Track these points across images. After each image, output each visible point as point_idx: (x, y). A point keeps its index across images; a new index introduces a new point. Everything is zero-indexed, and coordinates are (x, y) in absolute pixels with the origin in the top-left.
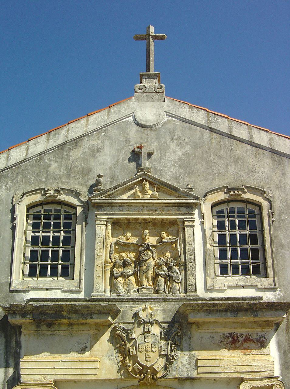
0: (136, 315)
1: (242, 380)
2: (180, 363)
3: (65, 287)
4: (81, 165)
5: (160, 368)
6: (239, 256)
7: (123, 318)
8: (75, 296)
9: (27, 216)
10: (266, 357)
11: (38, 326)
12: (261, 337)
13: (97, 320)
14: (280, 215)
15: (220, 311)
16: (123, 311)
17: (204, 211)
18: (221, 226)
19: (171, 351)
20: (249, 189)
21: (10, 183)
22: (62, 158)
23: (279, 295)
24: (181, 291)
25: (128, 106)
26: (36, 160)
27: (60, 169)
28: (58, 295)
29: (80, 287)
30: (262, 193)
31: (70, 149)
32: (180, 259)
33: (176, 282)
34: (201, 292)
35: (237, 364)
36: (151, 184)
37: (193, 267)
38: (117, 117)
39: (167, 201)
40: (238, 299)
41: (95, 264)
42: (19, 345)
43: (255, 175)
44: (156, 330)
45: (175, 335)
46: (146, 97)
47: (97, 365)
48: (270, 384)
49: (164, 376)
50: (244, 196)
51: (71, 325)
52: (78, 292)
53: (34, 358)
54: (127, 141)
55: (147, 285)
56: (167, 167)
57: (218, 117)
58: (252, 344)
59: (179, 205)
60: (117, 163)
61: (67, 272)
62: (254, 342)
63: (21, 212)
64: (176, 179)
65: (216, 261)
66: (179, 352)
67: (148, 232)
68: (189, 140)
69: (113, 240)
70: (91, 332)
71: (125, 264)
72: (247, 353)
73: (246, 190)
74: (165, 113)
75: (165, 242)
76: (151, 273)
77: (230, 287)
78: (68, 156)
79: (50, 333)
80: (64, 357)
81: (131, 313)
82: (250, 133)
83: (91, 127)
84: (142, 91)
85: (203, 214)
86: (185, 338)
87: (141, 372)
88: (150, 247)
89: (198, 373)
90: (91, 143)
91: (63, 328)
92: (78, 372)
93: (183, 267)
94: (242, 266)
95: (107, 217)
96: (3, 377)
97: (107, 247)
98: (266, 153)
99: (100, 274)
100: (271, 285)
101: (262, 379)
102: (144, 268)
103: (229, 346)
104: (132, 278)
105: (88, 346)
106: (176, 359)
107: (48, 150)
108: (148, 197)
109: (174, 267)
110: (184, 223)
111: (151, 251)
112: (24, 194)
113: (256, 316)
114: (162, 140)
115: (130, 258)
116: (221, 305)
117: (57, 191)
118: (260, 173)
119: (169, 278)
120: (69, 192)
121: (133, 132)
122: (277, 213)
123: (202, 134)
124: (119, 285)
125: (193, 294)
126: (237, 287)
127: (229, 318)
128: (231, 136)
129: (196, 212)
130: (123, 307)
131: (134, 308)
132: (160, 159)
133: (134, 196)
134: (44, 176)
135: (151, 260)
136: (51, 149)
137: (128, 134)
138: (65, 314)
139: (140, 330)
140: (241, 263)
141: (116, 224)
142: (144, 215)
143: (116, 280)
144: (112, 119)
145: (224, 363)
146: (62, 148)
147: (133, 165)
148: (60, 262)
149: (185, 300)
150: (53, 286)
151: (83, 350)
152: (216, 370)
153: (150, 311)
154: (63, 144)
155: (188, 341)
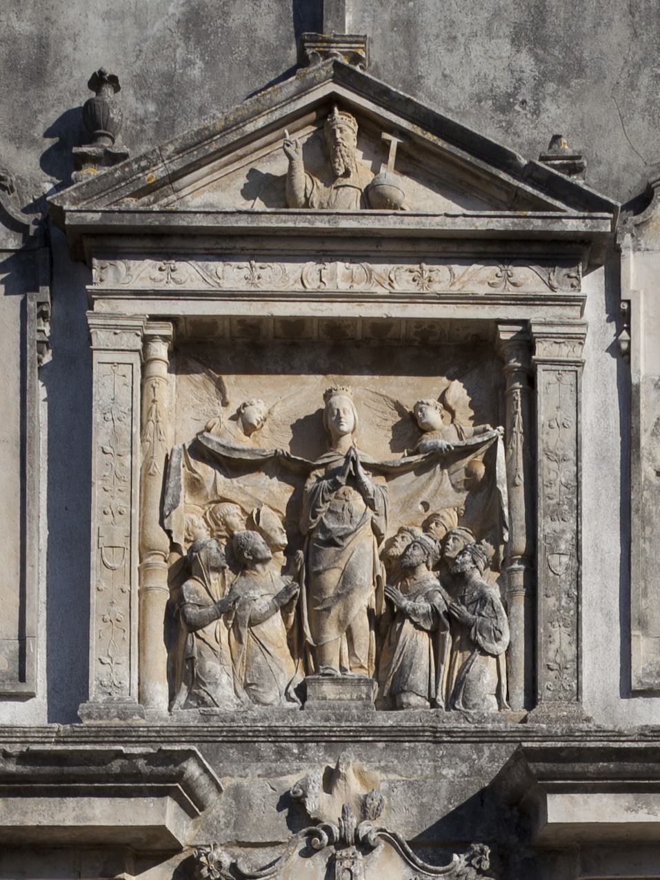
0: (293, 805)
17: (632, 286)
24: (508, 699)
29: (22, 678)
32: (506, 538)
36: (370, 130)
55: (346, 664)
76: (364, 599)
85: (629, 302)
88: (360, 469)
97: (147, 472)
99: (120, 503)
108: (350, 199)
110: (531, 349)
115: (262, 532)
124: (211, 665)
131: (283, 774)
143: (198, 636)
149: (527, 734)
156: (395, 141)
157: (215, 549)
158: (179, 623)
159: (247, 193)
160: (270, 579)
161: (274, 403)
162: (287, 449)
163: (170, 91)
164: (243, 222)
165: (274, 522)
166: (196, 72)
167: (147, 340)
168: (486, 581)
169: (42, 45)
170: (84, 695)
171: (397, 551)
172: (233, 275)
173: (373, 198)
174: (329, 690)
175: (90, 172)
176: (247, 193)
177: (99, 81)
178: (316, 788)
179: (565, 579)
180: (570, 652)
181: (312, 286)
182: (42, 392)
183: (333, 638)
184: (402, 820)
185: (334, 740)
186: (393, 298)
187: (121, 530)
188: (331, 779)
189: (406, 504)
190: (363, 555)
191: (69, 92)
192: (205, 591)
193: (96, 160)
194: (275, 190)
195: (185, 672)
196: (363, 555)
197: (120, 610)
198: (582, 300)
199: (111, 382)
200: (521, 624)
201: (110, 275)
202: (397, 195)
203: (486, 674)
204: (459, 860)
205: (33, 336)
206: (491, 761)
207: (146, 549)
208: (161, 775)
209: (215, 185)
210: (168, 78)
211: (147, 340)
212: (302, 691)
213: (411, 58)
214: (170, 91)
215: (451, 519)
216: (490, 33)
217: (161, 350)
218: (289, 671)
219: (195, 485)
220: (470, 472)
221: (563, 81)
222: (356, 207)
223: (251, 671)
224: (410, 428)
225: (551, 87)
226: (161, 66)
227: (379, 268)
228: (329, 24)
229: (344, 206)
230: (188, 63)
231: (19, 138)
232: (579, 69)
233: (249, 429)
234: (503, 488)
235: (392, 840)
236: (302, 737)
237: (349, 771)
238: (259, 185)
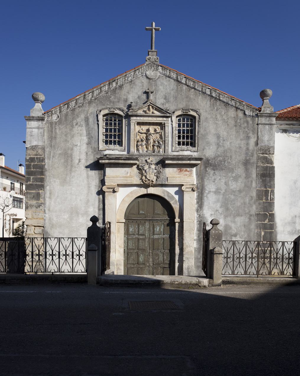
0: (146, 161)
47: (132, 179)
76: (152, 144)
97: (135, 134)
99: (133, 136)
108: (151, 113)
124: (140, 149)
152: (174, 181)
156: (154, 108)
157: (140, 140)
158: (137, 146)
159: (143, 112)
160: (144, 142)
161: (144, 128)
162: (146, 132)
163: (137, 103)
164: (143, 115)
165: (145, 138)
166: (139, 101)
167: (135, 123)
168: (161, 143)
169: (127, 99)
170: (130, 152)
171: (154, 140)
172: (142, 118)
173: (153, 113)
174: (149, 151)
175: (131, 110)
176: (143, 112)
177: (131, 103)
178: (148, 159)
179: (167, 143)
180: (168, 149)
181: (148, 119)
182: (127, 127)
183: (149, 147)
184: (154, 162)
185: (149, 156)
186: (154, 120)
187: (133, 139)
188: (149, 159)
189: (155, 136)
190: (152, 141)
191: (129, 103)
192: (139, 143)
193: (131, 109)
194: (145, 112)
195: (138, 150)
196: (152, 141)
197: (133, 145)
198: (169, 121)
199: (132, 127)
200: (164, 146)
201: (132, 118)
202: (155, 113)
203: (161, 150)
204: (159, 165)
205: (126, 123)
206: (162, 158)
207: (135, 140)
208: (137, 159)
209: (140, 111)
210: (136, 102)
211: (135, 123)
212: (147, 151)
213: (156, 100)
214: (137, 103)
215: (158, 138)
216: (162, 99)
217: (136, 124)
218: (146, 150)
219: (138, 135)
220: (160, 134)
221: (168, 102)
222: (151, 113)
223: (143, 150)
224: (155, 130)
225: (167, 103)
226: (136, 101)
227: (153, 118)
228: (149, 98)
229: (150, 113)
230: (138, 101)
231: (125, 106)
232: (169, 101)
233: (143, 130)
234: (163, 135)
235: (154, 164)
236: (147, 155)
237: (150, 158)
238: (144, 111)
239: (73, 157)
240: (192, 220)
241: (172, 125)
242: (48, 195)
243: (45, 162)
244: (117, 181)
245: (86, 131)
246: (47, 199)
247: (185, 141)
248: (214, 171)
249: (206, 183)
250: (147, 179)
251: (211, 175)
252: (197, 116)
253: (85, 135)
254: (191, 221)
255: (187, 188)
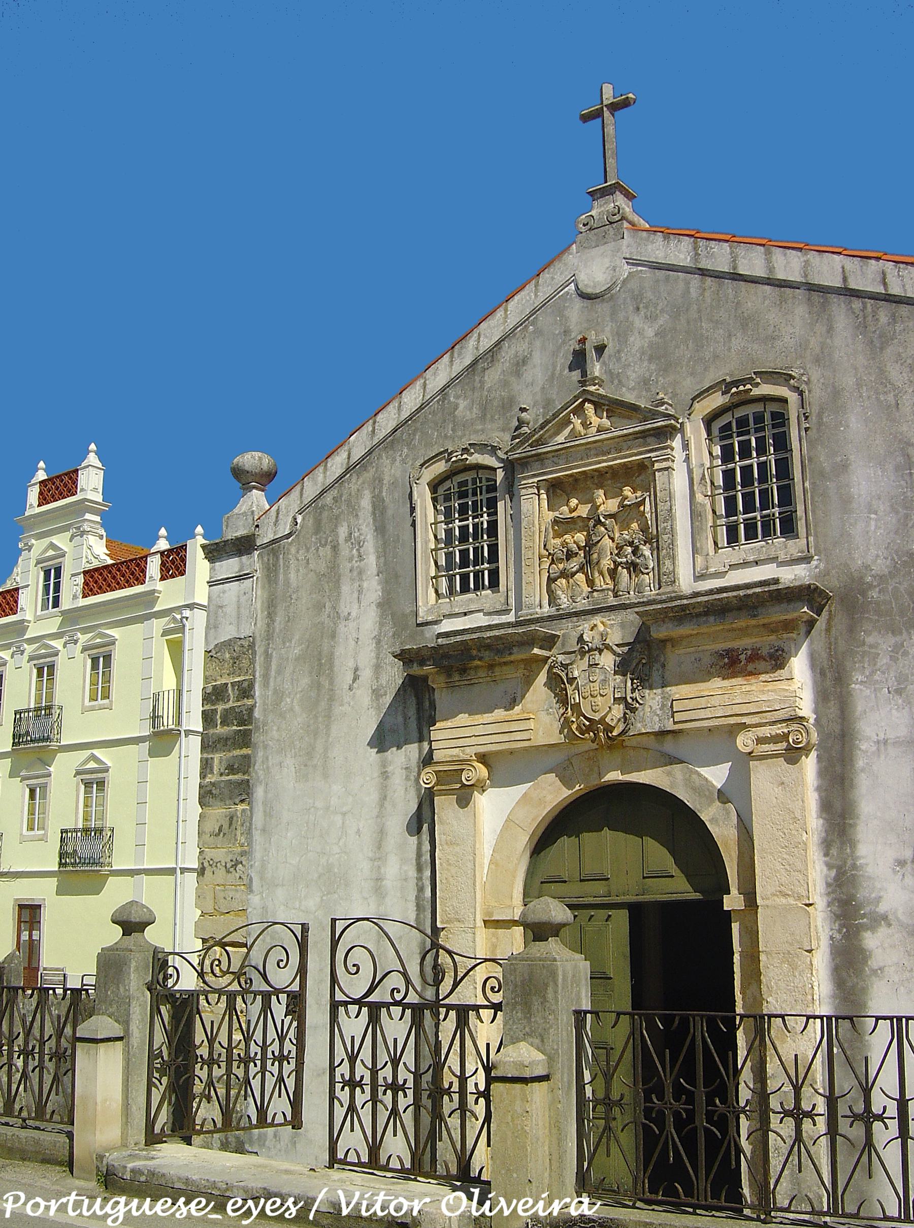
1: (744, 726)
2: (648, 709)
3: (488, 607)
4: (501, 395)
5: (615, 721)
6: (758, 505)
7: (563, 645)
8: (504, 619)
9: (435, 500)
10: (783, 685)
11: (449, 676)
12: (777, 650)
13: (518, 655)
14: (820, 415)
15: (698, 615)
16: (564, 635)
18: (727, 456)
19: (633, 690)
20: (762, 376)
21: (406, 450)
22: (473, 389)
23: (816, 567)
25: (565, 264)
26: (438, 401)
27: (471, 409)
28: (481, 620)
30: (784, 378)
31: (484, 370)
33: (643, 573)
34: (686, 582)
35: (734, 702)
36: (597, 406)
37: (670, 541)
38: (549, 291)
39: (621, 433)
40: (748, 586)
41: (523, 564)
42: (433, 706)
43: (779, 343)
44: (607, 661)
45: (637, 664)
46: (594, 238)
47: (531, 724)
48: (786, 731)
49: (623, 732)
50: (756, 392)
51: (491, 667)
52: (507, 611)
53: (449, 724)
54: (566, 332)
56: (630, 365)
57: (713, 243)
58: (761, 665)
59: (644, 435)
60: (552, 377)
61: (494, 583)
62: (765, 660)
63: (423, 496)
64: (645, 384)
65: (719, 522)
66: (648, 691)
67: (601, 492)
68: (666, 303)
69: (550, 516)
70: (520, 672)
71: (570, 555)
72: (753, 681)
73: (758, 380)
74: (624, 261)
75: (626, 505)
77: (733, 567)
78: (482, 382)
79: (467, 683)
80: (487, 718)
81: (575, 635)
82: (768, 261)
83: (512, 322)
84: (588, 227)
86: (657, 666)
87: (589, 729)
89: (675, 723)
90: (512, 352)
91: (482, 673)
92: (506, 738)
93: (655, 544)
94: (762, 522)
95: (536, 480)
96: (417, 756)
98: (799, 294)
100: (802, 552)
101: (773, 723)
102: (595, 556)
103: (724, 672)
104: (580, 577)
105: (519, 695)
106: (641, 702)
107: (453, 380)
109: (641, 547)
111: (603, 525)
112: (693, 399)
113: (755, 616)
114: (621, 316)
116: (693, 606)
117: (465, 451)
118: (787, 339)
119: (633, 568)
120: (482, 448)
121: (576, 311)
122: (814, 411)
123: (688, 283)
124: (559, 592)
125: (670, 589)
126: (745, 564)
127: (712, 626)
128: (736, 277)
129: (677, 443)
130: (566, 630)
132: (619, 351)
133: (574, 435)
134: (451, 426)
135: (607, 541)
136: (457, 377)
137: (567, 319)
138: (474, 652)
139: (584, 664)
140: (761, 517)
141: (557, 490)
142: (551, 472)
144: (542, 297)
145: (714, 701)
146: (473, 370)
147: (576, 375)
148: (486, 565)
150: (473, 607)
151: (512, 703)
152: (702, 714)
153: (601, 628)
154: (474, 363)
155: (661, 670)
239: (337, 662)
240: (799, 898)
241: (688, 468)
242: (258, 819)
243: (253, 697)
244: (473, 741)
245: (378, 558)
246: (257, 836)
247: (755, 518)
248: (898, 639)
249: (860, 706)
250: (585, 717)
251: (883, 661)
252: (793, 398)
253: (375, 573)
254: (791, 901)
255: (760, 741)
